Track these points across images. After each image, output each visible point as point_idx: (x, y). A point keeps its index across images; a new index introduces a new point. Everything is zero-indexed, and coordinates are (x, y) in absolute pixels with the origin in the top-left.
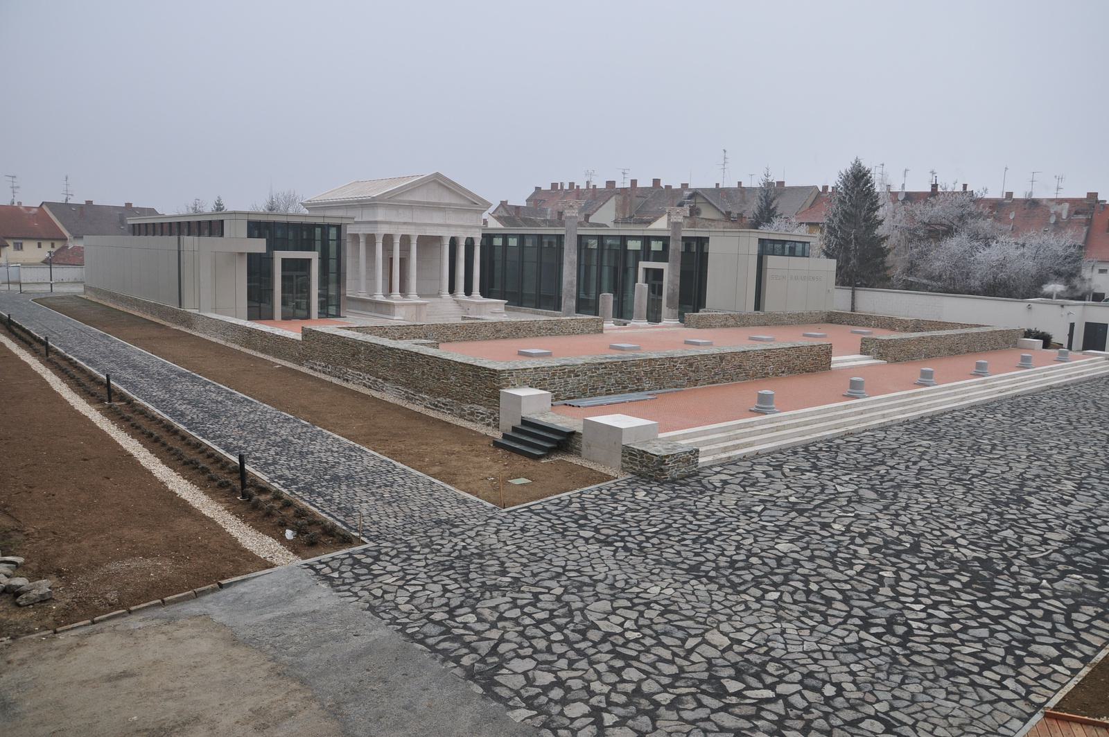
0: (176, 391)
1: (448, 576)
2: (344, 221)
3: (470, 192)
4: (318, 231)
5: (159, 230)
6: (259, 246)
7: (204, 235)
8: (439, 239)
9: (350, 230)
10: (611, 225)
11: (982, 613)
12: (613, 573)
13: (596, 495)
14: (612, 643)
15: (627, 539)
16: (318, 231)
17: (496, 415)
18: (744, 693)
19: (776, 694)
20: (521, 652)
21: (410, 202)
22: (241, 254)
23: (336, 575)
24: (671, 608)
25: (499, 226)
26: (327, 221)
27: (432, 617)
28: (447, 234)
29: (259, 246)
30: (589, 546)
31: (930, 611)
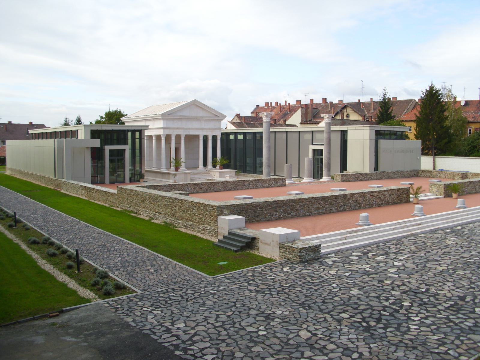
0: (50, 221)
1: (175, 307)
2: (143, 128)
3: (214, 110)
4: (129, 134)
5: (41, 136)
6: (97, 143)
7: (68, 138)
8: (197, 136)
9: (147, 133)
10: (299, 125)
11: (450, 321)
12: (260, 305)
13: (262, 270)
14: (250, 336)
15: (272, 290)
16: (129, 134)
17: (216, 230)
18: (312, 357)
19: (328, 358)
20: (204, 340)
21: (180, 116)
22: (87, 148)
23: (119, 306)
24: (286, 320)
25: (234, 128)
26: (134, 129)
27: (164, 324)
28: (201, 134)
29: (97, 143)
30: (251, 293)
31: (422, 320)
